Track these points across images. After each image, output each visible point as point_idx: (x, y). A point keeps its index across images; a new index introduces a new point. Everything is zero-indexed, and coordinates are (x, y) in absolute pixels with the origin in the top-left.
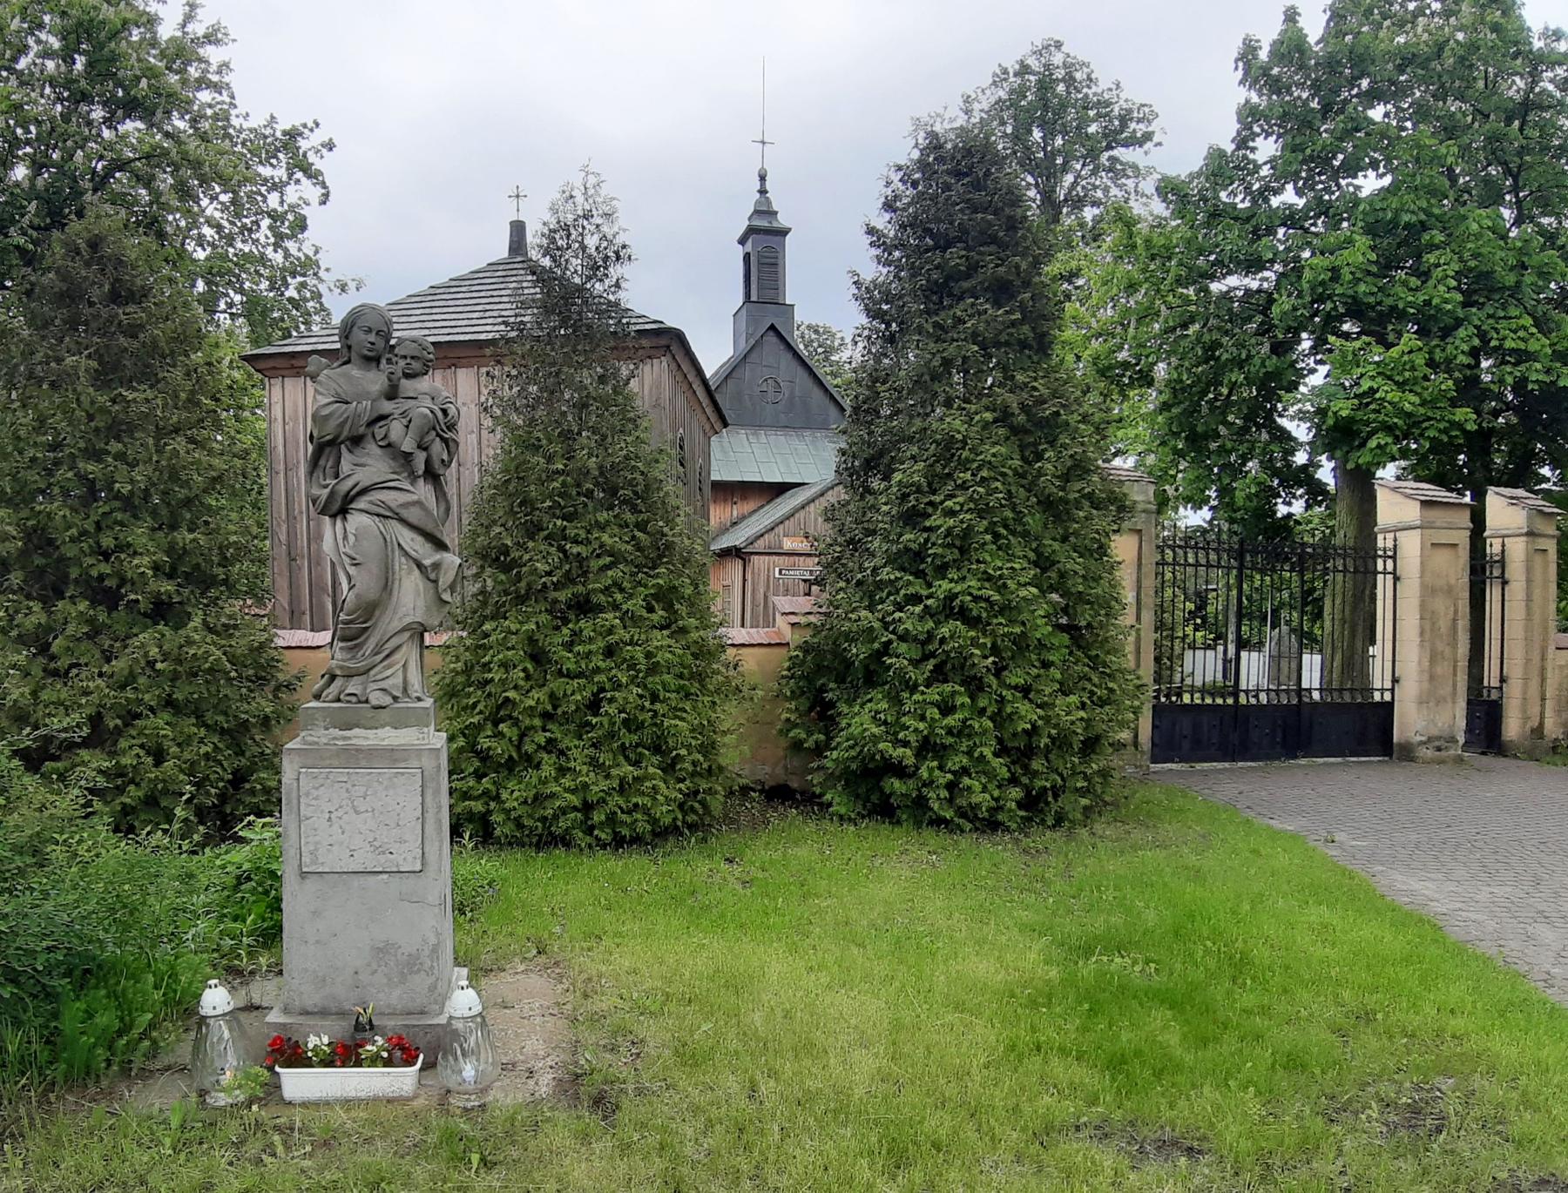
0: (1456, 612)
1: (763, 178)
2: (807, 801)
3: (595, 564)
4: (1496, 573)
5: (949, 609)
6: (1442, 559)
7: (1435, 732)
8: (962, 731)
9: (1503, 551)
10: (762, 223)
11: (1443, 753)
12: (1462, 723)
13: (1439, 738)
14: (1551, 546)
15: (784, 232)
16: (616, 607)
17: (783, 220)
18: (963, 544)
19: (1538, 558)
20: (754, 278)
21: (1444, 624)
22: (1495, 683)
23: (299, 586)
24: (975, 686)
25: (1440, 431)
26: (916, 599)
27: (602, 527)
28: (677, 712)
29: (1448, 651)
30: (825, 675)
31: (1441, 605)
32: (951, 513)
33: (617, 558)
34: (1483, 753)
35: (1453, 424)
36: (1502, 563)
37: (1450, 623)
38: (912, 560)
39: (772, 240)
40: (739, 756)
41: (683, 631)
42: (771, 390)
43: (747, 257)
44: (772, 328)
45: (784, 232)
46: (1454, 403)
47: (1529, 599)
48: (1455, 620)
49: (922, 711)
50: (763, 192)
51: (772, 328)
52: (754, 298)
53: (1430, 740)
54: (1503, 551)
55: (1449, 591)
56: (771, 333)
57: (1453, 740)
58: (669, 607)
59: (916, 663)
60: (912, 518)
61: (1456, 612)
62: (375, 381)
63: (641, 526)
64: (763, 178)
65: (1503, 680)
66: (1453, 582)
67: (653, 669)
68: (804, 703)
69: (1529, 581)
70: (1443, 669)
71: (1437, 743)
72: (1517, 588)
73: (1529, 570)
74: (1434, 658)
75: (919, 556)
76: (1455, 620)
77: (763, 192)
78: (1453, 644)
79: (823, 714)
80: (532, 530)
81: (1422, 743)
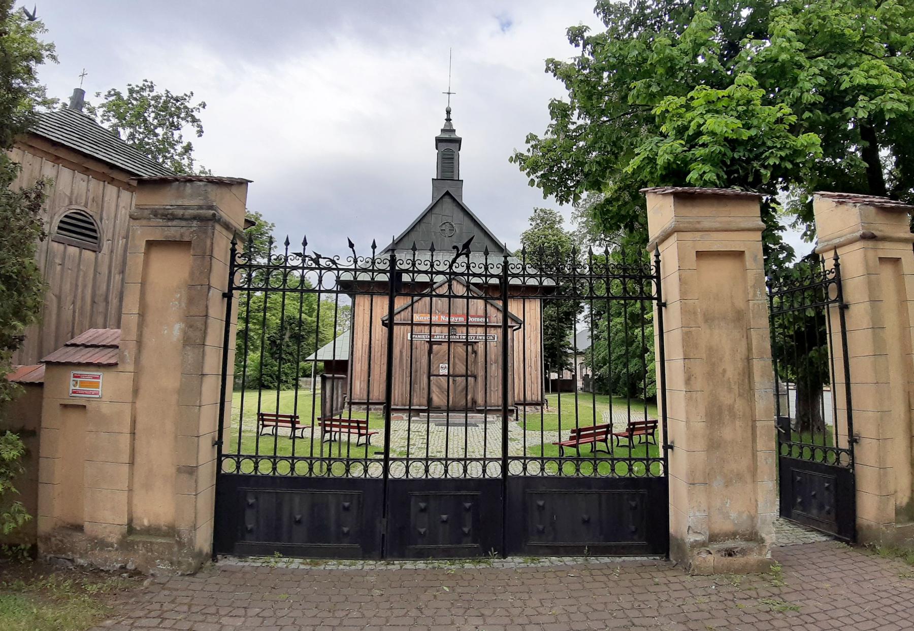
0: (749, 349)
1: (448, 112)
4: (833, 295)
6: (719, 274)
7: (722, 525)
9: (837, 265)
10: (446, 136)
11: (738, 560)
13: (733, 535)
17: (458, 134)
19: (887, 272)
21: (731, 369)
22: (844, 444)
23: (87, 369)
25: (781, 158)
29: (740, 405)
31: (724, 339)
34: (836, 539)
35: (796, 152)
36: (838, 280)
37: (740, 365)
39: (452, 146)
42: (447, 231)
44: (447, 193)
46: (794, 130)
47: (877, 327)
48: (749, 359)
50: (448, 120)
51: (447, 193)
53: (713, 538)
54: (837, 265)
55: (739, 318)
56: (447, 199)
61: (749, 349)
64: (448, 112)
65: (853, 440)
66: (740, 304)
69: (874, 301)
70: (733, 432)
71: (730, 544)
72: (859, 314)
73: (872, 286)
74: (715, 415)
76: (749, 359)
77: (448, 120)
81: (696, 545)
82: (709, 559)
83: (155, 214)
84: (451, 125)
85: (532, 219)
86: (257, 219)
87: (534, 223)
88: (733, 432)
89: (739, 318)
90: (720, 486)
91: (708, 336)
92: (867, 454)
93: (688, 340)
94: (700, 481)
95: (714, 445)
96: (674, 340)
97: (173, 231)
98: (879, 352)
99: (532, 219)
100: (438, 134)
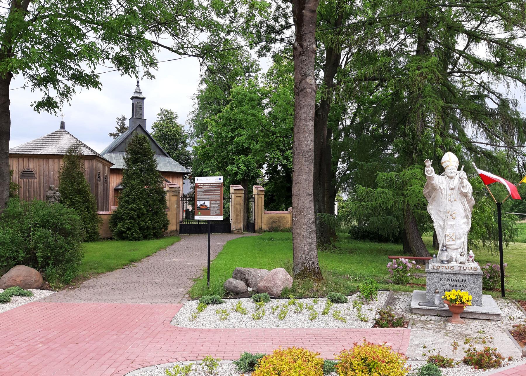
2: (111, 239)
3: (76, 203)
5: (132, 209)
6: (238, 199)
7: (237, 228)
8: (133, 226)
10: (137, 95)
12: (242, 227)
14: (263, 196)
15: (143, 99)
16: (79, 209)
18: (134, 200)
19: (260, 198)
20: (134, 111)
21: (239, 210)
24: (135, 220)
26: (127, 208)
27: (78, 197)
28: (88, 224)
30: (116, 218)
31: (238, 206)
32: (132, 196)
33: (80, 202)
38: (127, 202)
39: (140, 101)
40: (101, 231)
41: (90, 212)
43: (133, 104)
44: (140, 126)
45: (143, 99)
47: (258, 205)
49: (128, 223)
51: (140, 126)
52: (134, 117)
55: (240, 204)
56: (139, 129)
57: (241, 230)
58: (88, 209)
59: (127, 217)
60: (128, 196)
62: (53, 192)
63: (84, 197)
67: (85, 218)
68: (113, 224)
70: (239, 217)
74: (237, 215)
75: (128, 201)
77: (138, 86)
78: (241, 213)
79: (115, 225)
80: (66, 198)
82: (236, 232)
83: (173, 191)
84: (139, 89)
85: (159, 115)
86: (277, 228)
87: (160, 117)
88: (239, 217)
89: (240, 204)
90: (237, 223)
91: (236, 206)
92: (256, 221)
93: (234, 207)
94: (235, 223)
95: (237, 219)
96: (233, 206)
97: (175, 194)
98: (258, 208)
99: (159, 115)
100: (132, 95)
